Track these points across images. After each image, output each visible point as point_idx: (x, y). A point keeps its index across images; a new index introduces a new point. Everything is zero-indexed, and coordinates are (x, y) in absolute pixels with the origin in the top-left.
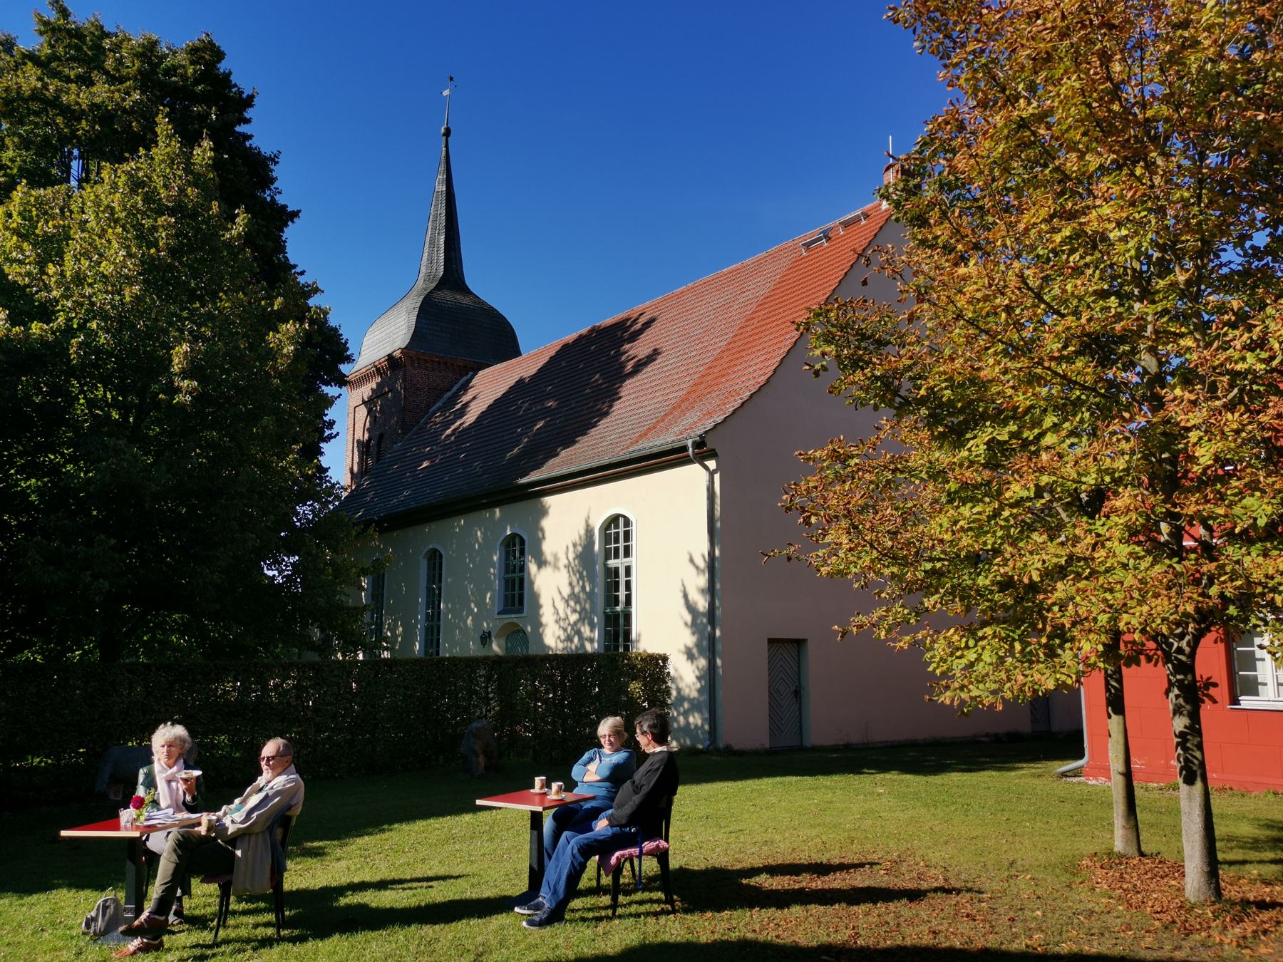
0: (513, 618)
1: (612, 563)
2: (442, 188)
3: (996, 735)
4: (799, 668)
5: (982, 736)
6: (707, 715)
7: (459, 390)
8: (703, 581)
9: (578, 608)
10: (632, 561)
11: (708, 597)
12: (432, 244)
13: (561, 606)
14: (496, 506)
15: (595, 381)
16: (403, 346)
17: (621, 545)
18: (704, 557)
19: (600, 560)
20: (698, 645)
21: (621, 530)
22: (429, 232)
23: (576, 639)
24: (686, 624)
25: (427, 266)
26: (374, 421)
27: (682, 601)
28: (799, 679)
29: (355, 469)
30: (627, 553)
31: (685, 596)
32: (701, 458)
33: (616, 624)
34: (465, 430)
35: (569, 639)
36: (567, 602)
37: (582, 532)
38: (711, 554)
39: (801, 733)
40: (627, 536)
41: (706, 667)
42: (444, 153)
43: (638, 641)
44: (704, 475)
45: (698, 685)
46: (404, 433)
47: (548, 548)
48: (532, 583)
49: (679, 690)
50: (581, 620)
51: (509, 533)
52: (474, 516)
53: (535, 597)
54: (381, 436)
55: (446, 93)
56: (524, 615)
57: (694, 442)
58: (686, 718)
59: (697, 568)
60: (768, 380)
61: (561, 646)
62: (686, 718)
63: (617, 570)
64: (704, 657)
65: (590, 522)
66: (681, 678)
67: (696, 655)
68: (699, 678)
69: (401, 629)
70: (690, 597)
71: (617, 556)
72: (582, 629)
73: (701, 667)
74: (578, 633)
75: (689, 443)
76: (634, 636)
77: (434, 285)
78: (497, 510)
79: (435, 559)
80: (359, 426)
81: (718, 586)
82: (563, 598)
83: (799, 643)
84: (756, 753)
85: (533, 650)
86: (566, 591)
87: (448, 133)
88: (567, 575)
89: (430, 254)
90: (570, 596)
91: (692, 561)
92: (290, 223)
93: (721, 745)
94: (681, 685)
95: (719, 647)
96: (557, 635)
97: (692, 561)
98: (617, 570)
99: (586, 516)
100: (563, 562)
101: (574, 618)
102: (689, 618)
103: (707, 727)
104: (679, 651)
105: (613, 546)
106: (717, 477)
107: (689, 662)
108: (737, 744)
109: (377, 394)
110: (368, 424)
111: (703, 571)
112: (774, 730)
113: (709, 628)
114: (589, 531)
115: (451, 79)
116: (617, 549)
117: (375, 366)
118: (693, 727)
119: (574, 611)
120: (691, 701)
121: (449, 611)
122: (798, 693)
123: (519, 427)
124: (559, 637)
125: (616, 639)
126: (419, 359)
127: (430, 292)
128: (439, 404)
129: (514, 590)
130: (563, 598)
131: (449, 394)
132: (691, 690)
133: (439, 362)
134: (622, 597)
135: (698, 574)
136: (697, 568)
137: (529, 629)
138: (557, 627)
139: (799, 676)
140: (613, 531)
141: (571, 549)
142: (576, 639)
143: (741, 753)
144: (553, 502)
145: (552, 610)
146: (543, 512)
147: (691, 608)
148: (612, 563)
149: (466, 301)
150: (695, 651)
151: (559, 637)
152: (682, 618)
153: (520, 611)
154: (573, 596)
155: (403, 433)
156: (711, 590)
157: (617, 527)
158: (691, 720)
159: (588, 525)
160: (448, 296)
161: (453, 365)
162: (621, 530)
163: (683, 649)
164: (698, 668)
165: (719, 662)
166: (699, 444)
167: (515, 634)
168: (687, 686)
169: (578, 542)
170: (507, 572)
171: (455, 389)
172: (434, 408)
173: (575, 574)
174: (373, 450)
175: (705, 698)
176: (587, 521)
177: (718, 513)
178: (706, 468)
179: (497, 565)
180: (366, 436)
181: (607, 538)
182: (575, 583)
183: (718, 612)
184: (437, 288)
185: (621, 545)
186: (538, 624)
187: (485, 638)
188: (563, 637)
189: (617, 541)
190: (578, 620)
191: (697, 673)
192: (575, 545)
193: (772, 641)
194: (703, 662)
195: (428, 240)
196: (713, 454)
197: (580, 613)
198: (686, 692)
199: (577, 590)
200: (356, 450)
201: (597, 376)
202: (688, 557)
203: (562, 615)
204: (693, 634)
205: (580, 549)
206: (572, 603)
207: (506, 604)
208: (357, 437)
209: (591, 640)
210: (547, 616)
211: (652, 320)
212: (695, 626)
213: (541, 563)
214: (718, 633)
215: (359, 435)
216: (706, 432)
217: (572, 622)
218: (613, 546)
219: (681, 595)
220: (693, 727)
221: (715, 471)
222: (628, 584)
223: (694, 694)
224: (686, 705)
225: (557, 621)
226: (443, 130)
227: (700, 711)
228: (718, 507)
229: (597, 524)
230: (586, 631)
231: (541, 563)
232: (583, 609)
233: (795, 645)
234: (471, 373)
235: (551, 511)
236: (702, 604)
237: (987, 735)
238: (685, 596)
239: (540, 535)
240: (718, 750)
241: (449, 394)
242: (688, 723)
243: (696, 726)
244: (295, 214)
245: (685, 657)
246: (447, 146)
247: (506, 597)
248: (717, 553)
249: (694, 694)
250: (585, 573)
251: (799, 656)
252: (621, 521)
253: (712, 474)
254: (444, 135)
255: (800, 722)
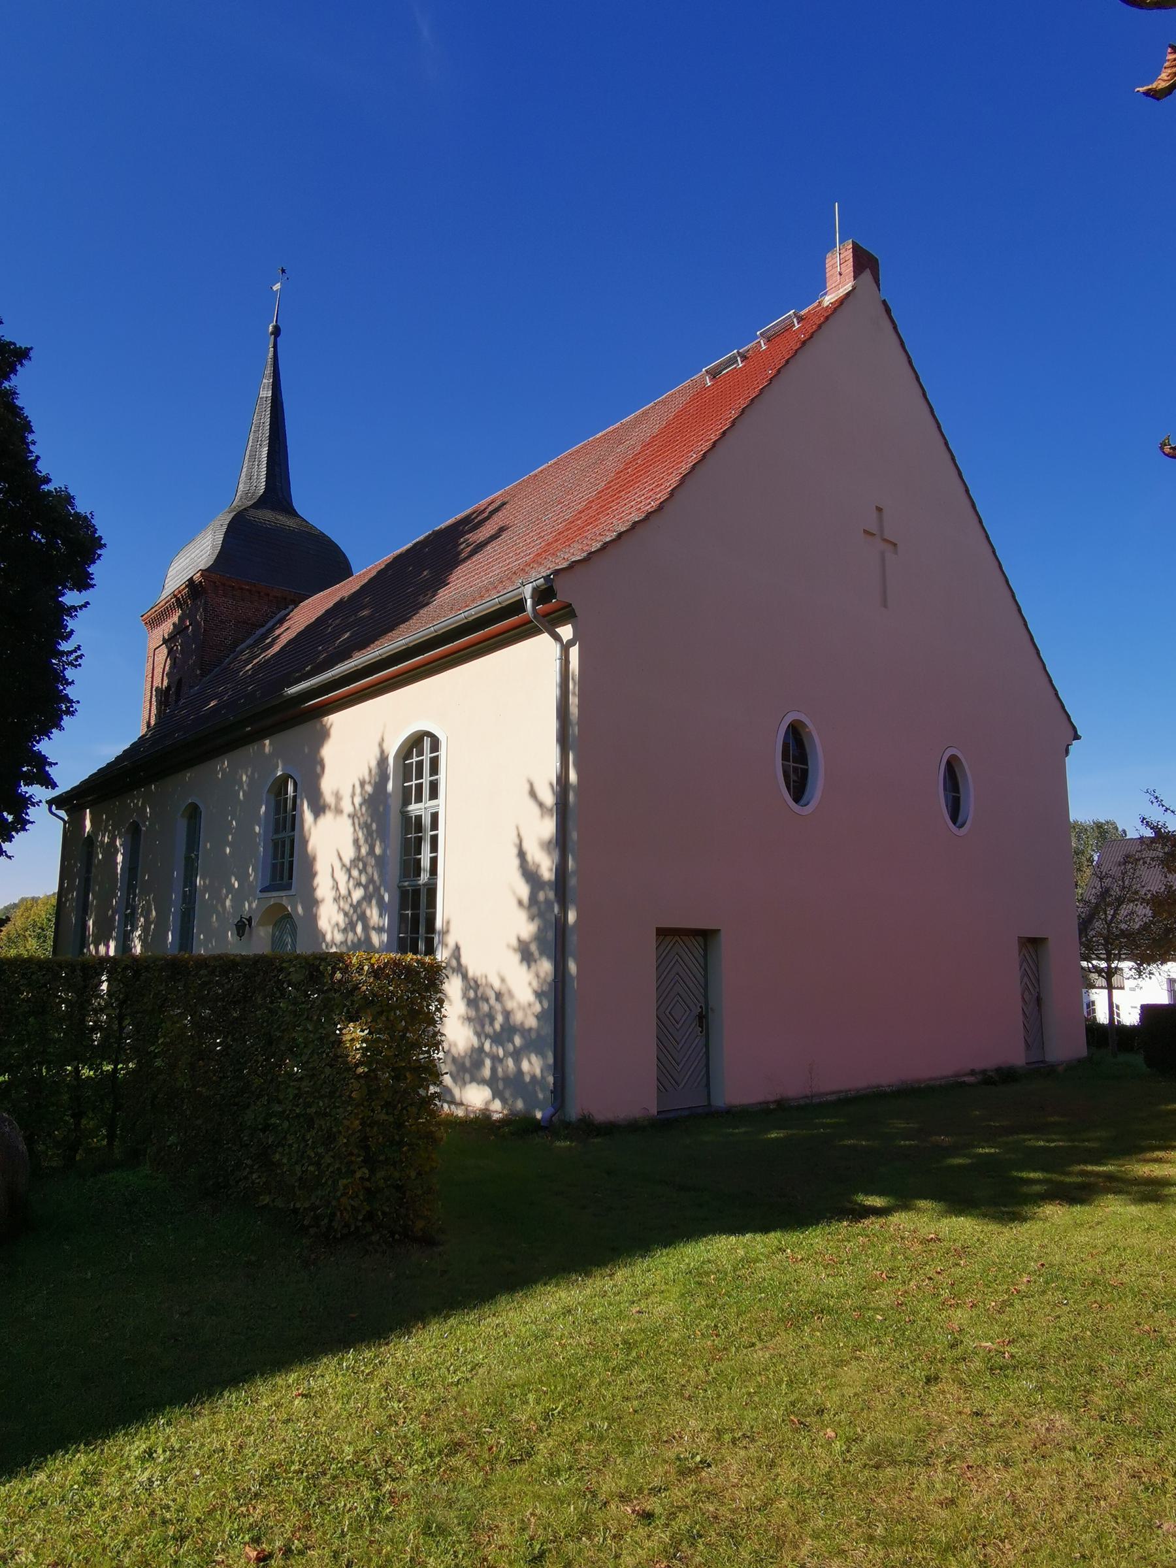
0: (274, 897)
1: (414, 808)
2: (266, 393)
3: (984, 1072)
4: (706, 977)
5: (966, 1075)
6: (551, 1060)
7: (276, 624)
8: (548, 828)
9: (364, 880)
10: (440, 804)
11: (556, 855)
12: (253, 457)
13: (342, 877)
14: (265, 737)
15: (425, 576)
16: (204, 568)
17: (426, 780)
18: (551, 785)
19: (395, 804)
20: (539, 938)
21: (427, 757)
22: (250, 444)
23: (359, 929)
24: (520, 903)
25: (245, 483)
26: (174, 665)
27: (515, 862)
28: (706, 997)
29: (153, 723)
30: (434, 794)
31: (522, 855)
32: (548, 623)
33: (416, 906)
34: (268, 659)
35: (351, 926)
36: (349, 871)
37: (374, 764)
38: (563, 778)
39: (708, 1085)
40: (434, 769)
41: (550, 978)
42: (271, 354)
43: (446, 932)
44: (555, 649)
45: (537, 1008)
46: (202, 675)
47: (328, 785)
48: (305, 842)
49: (507, 1014)
50: (367, 898)
51: (279, 773)
52: (240, 754)
53: (309, 864)
54: (180, 681)
55: (277, 287)
56: (292, 892)
57: (535, 590)
58: (518, 1062)
59: (541, 805)
60: (661, 507)
61: (339, 937)
62: (518, 1062)
63: (419, 818)
64: (549, 958)
65: (385, 746)
66: (510, 992)
67: (536, 954)
68: (539, 995)
69: (154, 913)
70: (529, 858)
71: (419, 799)
72: (368, 912)
73: (542, 975)
74: (363, 918)
75: (528, 591)
76: (439, 924)
77: (252, 502)
78: (267, 742)
79: (194, 813)
80: (158, 671)
81: (574, 835)
82: (344, 865)
83: (706, 936)
84: (633, 1127)
85: (303, 948)
86: (349, 854)
87: (277, 332)
88: (352, 829)
89: (250, 468)
90: (352, 861)
91: (533, 794)
92: (19, 367)
93: (573, 1112)
94: (510, 1005)
95: (573, 940)
96: (333, 922)
97: (533, 794)
98: (419, 818)
99: (378, 739)
100: (347, 807)
101: (358, 894)
102: (524, 891)
103: (551, 1079)
104: (508, 946)
105: (414, 782)
106: (574, 652)
107: (524, 967)
108: (602, 1113)
109: (179, 630)
110: (167, 668)
111: (551, 810)
112: (666, 1079)
113: (556, 909)
114: (383, 761)
115: (283, 271)
116: (419, 787)
117: (175, 596)
118: (527, 1079)
119: (358, 884)
120: (524, 1032)
121: (206, 888)
122: (703, 1019)
123: (319, 646)
124: (337, 925)
125: (415, 929)
126: (224, 585)
127: (245, 509)
128: (249, 641)
129: (283, 857)
130: (344, 865)
131: (263, 630)
132: (526, 1016)
133: (250, 591)
134: (425, 863)
135: (542, 816)
136: (541, 805)
137: (300, 910)
138: (336, 907)
139: (706, 987)
140: (415, 759)
141: (358, 790)
142: (359, 929)
143: (609, 1130)
144: (337, 721)
145: (330, 883)
146: (324, 735)
147: (529, 874)
148: (414, 808)
149: (290, 522)
150: (533, 948)
151: (337, 925)
152: (514, 893)
153: (289, 887)
154: (358, 859)
155: (202, 675)
156: (561, 843)
157: (421, 753)
158: (525, 1066)
159: (382, 752)
160: (267, 516)
161: (268, 595)
162: (427, 757)
163: (514, 943)
164: (538, 976)
165: (572, 967)
166: (544, 594)
167: (283, 920)
168: (520, 1007)
169: (367, 778)
170: (276, 831)
171: (270, 624)
172: (243, 646)
173: (361, 828)
174: (172, 699)
175: (548, 1030)
176: (381, 745)
177: (574, 710)
178: (557, 638)
179: (263, 822)
180: (165, 683)
181: (406, 772)
182: (362, 841)
183: (573, 882)
184: (255, 506)
185: (426, 780)
186: (312, 903)
187: (243, 927)
188: (342, 925)
189: (420, 775)
190: (364, 898)
191: (535, 984)
192: (362, 784)
193: (662, 933)
194: (546, 967)
195: (248, 453)
196: (566, 614)
197: (366, 887)
198: (518, 1017)
199: (364, 851)
200: (154, 699)
201: (425, 573)
202: (527, 787)
203: (343, 891)
204: (532, 918)
205: (369, 789)
206: (355, 873)
207: (273, 878)
208: (155, 685)
209: (380, 930)
210: (323, 887)
211: (504, 504)
212: (534, 906)
213: (319, 809)
214: (572, 917)
215: (157, 683)
216: (557, 572)
217: (355, 902)
218: (414, 782)
219: (515, 851)
220: (527, 1079)
221: (571, 643)
222: (434, 840)
223: (532, 1022)
224: (518, 1041)
225: (335, 899)
226: (271, 328)
227: (540, 1053)
228: (574, 701)
229: (392, 750)
230: (373, 914)
231: (319, 809)
232: (371, 880)
233: (700, 939)
234: (291, 607)
235: (333, 732)
236: (546, 866)
237: (973, 1073)
238: (522, 855)
239: (319, 769)
240: (567, 1125)
241: (263, 630)
242: (520, 1072)
243: (533, 1077)
244: (23, 354)
245: (516, 957)
246: (275, 347)
247: (274, 866)
248: (573, 777)
249: (532, 1022)
250: (374, 826)
251: (705, 957)
252: (427, 742)
253: (565, 649)
254: (272, 333)
255: (707, 1066)
